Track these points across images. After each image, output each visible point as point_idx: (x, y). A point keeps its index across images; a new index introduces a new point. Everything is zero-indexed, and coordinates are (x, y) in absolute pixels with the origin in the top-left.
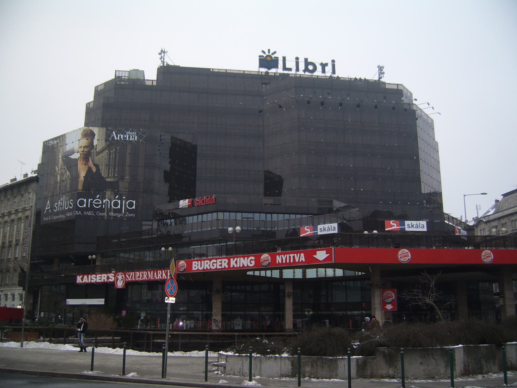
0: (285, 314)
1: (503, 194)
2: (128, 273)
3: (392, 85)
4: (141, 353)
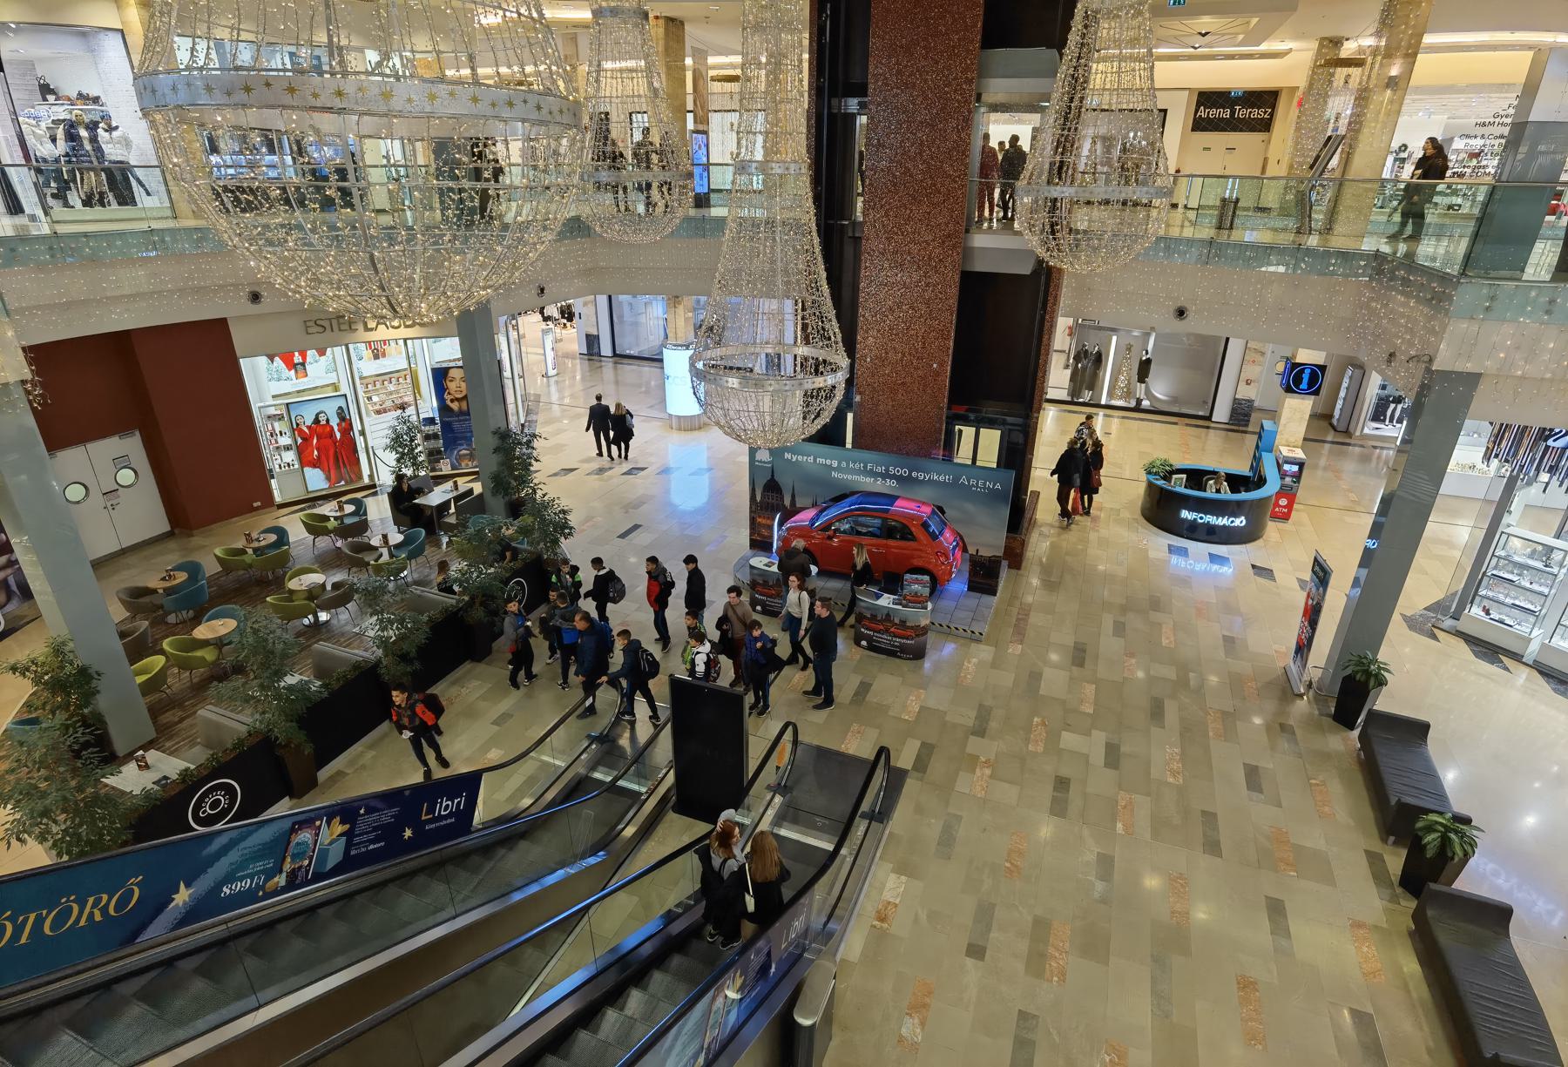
0: (143, 12)
3: (492, 898)
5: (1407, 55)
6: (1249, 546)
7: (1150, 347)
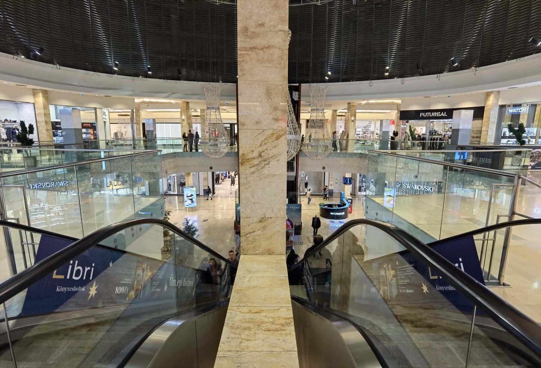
1: (238, 135)
2: (443, 115)
5: (354, 116)
7: (307, 179)
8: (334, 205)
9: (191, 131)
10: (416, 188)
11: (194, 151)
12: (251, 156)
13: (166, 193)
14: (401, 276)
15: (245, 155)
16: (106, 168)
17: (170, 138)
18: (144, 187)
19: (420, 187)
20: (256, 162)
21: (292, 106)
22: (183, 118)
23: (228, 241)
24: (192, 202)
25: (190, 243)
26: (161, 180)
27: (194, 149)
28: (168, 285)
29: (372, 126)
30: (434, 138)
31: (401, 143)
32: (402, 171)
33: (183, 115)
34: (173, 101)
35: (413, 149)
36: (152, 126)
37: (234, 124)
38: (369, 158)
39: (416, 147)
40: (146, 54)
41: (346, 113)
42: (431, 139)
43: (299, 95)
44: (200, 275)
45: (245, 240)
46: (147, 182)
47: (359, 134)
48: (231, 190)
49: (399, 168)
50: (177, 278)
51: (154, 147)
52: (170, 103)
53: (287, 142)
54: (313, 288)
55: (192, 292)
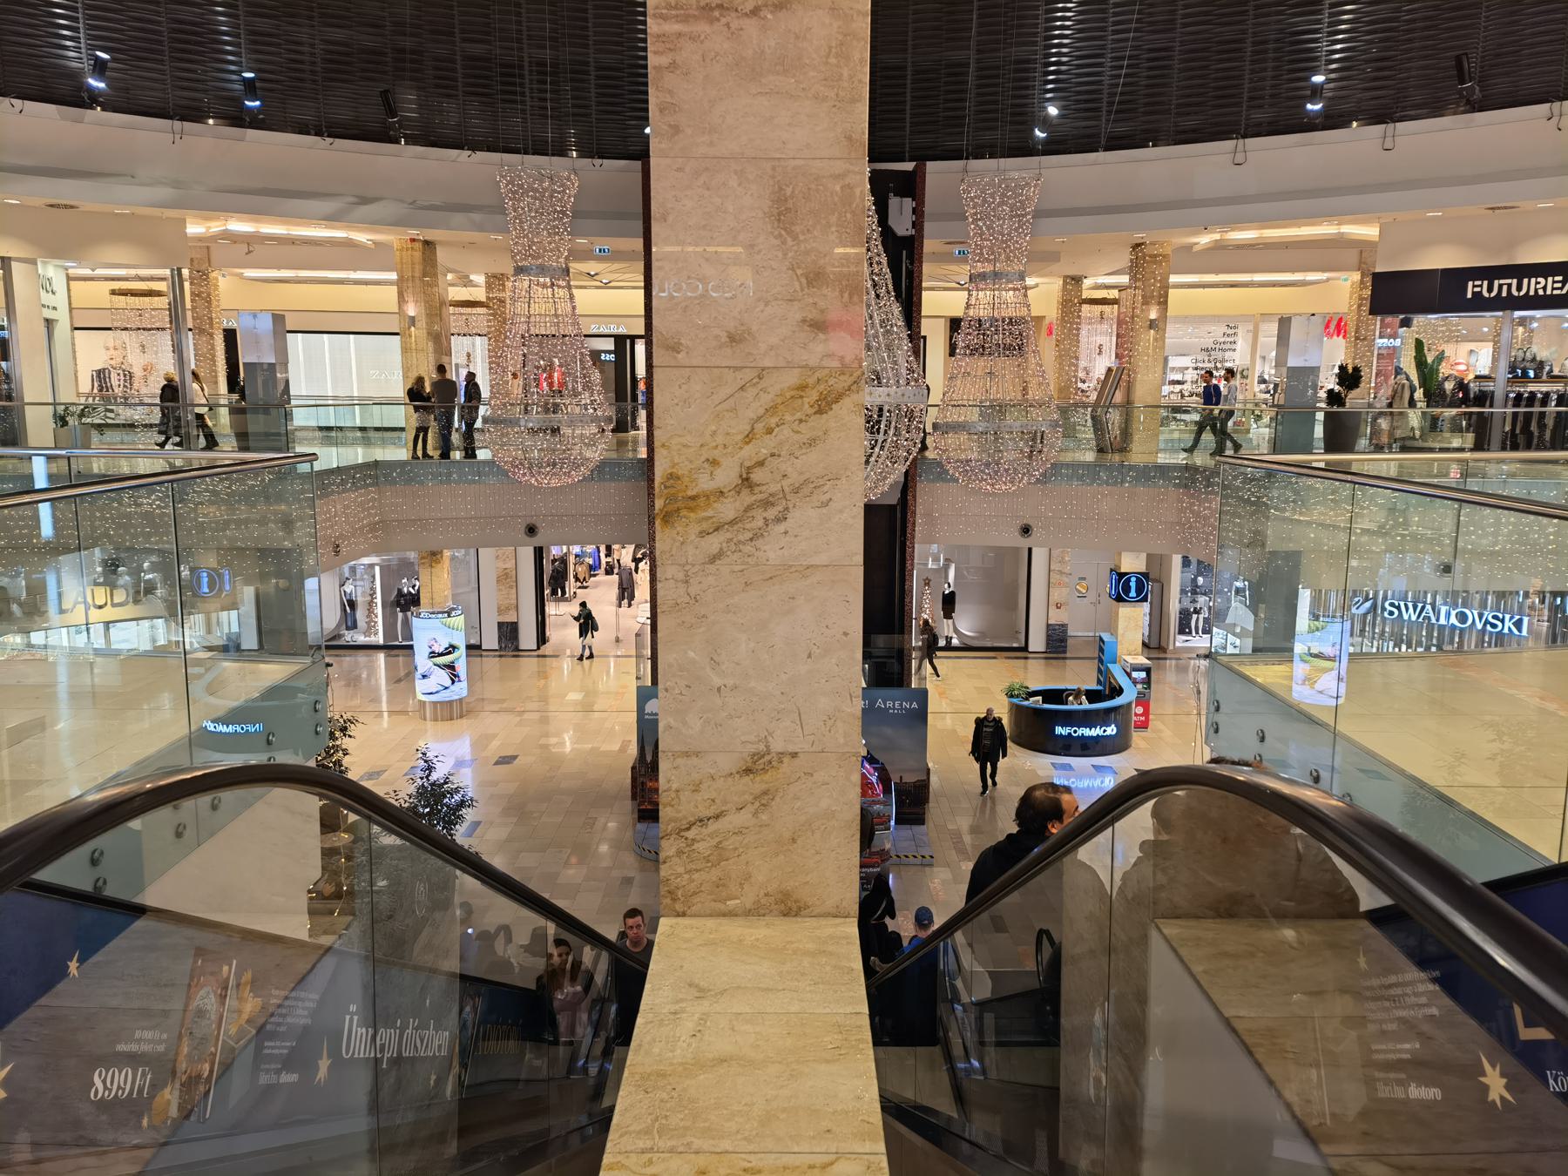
4: (1091, 859)
5: (1159, 303)
6: (1123, 754)
7: (951, 578)
8: (1069, 692)
9: (447, 367)
10: (1443, 621)
11: (457, 455)
12: (705, 483)
13: (334, 638)
14: (1381, 1022)
15: (678, 478)
16: (55, 528)
17: (352, 398)
18: (234, 614)
19: (1462, 617)
20: (727, 509)
21: (884, 260)
22: (411, 310)
23: (604, 848)
24: (454, 678)
25: (434, 862)
26: (311, 584)
27: (458, 449)
28: (335, 1053)
29: (1239, 346)
30: (1533, 394)
31: (1375, 419)
32: (1379, 544)
33: (410, 298)
34: (362, 237)
35: (1430, 444)
36: (268, 341)
37: (633, 338)
38: (1225, 487)
39: (1447, 435)
40: (236, 17)
41: (1121, 288)
42: (1518, 399)
43: (918, 212)
44: (479, 1001)
45: (680, 853)
46: (248, 593)
47: (1179, 382)
48: (618, 629)
49: (1365, 531)
50: (376, 1018)
51: (281, 439)
52: (349, 243)
53: (863, 421)
54: (981, 1061)
55: (440, 1081)
